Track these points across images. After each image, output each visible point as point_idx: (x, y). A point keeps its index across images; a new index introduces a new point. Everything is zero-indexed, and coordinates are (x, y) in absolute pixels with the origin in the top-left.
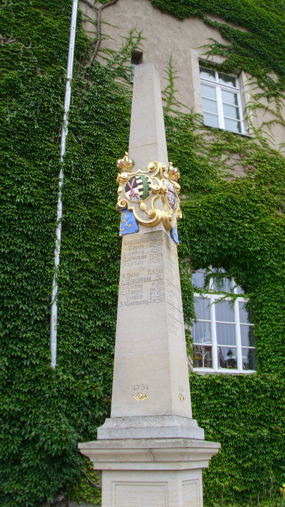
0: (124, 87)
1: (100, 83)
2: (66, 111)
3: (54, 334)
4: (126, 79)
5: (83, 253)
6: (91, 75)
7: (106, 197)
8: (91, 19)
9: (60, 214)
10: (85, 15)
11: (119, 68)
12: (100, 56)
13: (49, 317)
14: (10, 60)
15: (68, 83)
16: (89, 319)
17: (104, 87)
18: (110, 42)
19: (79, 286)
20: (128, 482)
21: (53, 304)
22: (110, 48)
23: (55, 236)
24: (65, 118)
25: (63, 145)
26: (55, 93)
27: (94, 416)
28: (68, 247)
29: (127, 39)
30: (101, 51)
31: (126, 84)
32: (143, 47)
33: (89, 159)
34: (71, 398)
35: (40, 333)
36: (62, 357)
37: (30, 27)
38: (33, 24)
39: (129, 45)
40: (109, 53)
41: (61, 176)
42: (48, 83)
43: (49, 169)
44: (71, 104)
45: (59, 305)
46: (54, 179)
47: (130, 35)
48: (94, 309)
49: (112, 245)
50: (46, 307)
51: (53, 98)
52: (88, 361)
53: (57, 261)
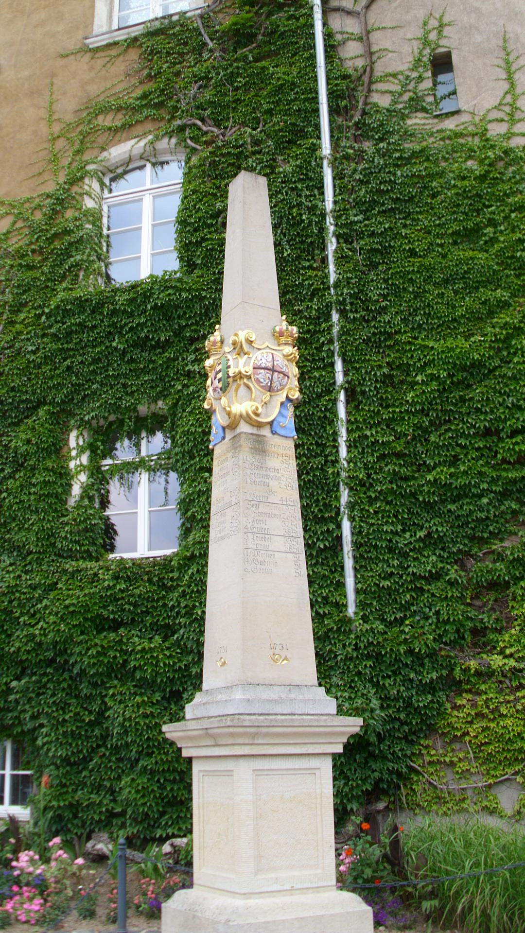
0: (425, 127)
1: (381, 140)
2: (328, 211)
3: (349, 563)
4: (427, 112)
5: (382, 429)
6: (362, 131)
7: (413, 327)
8: (352, 34)
9: (340, 378)
10: (341, 33)
11: (411, 99)
12: (377, 91)
13: (339, 539)
14: (234, 163)
15: (325, 162)
16: (404, 531)
17: (389, 144)
18: (390, 59)
19: (381, 482)
20: (300, 769)
21: (342, 519)
22: (390, 70)
23: (336, 415)
24: (329, 220)
25: (332, 267)
26: (307, 187)
27: (420, 681)
28: (358, 427)
29: (418, 39)
30: (377, 81)
31: (427, 122)
32: (451, 41)
33: (378, 275)
34: (378, 658)
35: (329, 566)
36: (362, 597)
37: (256, 95)
38: (260, 89)
39: (424, 48)
40: (391, 79)
41: (335, 317)
42: (293, 176)
43: (314, 312)
44: (335, 196)
45: (352, 519)
46: (324, 325)
47: (422, 30)
48: (410, 512)
49: (431, 404)
50: (332, 526)
51: (306, 196)
52: (408, 596)
53: (343, 452)
